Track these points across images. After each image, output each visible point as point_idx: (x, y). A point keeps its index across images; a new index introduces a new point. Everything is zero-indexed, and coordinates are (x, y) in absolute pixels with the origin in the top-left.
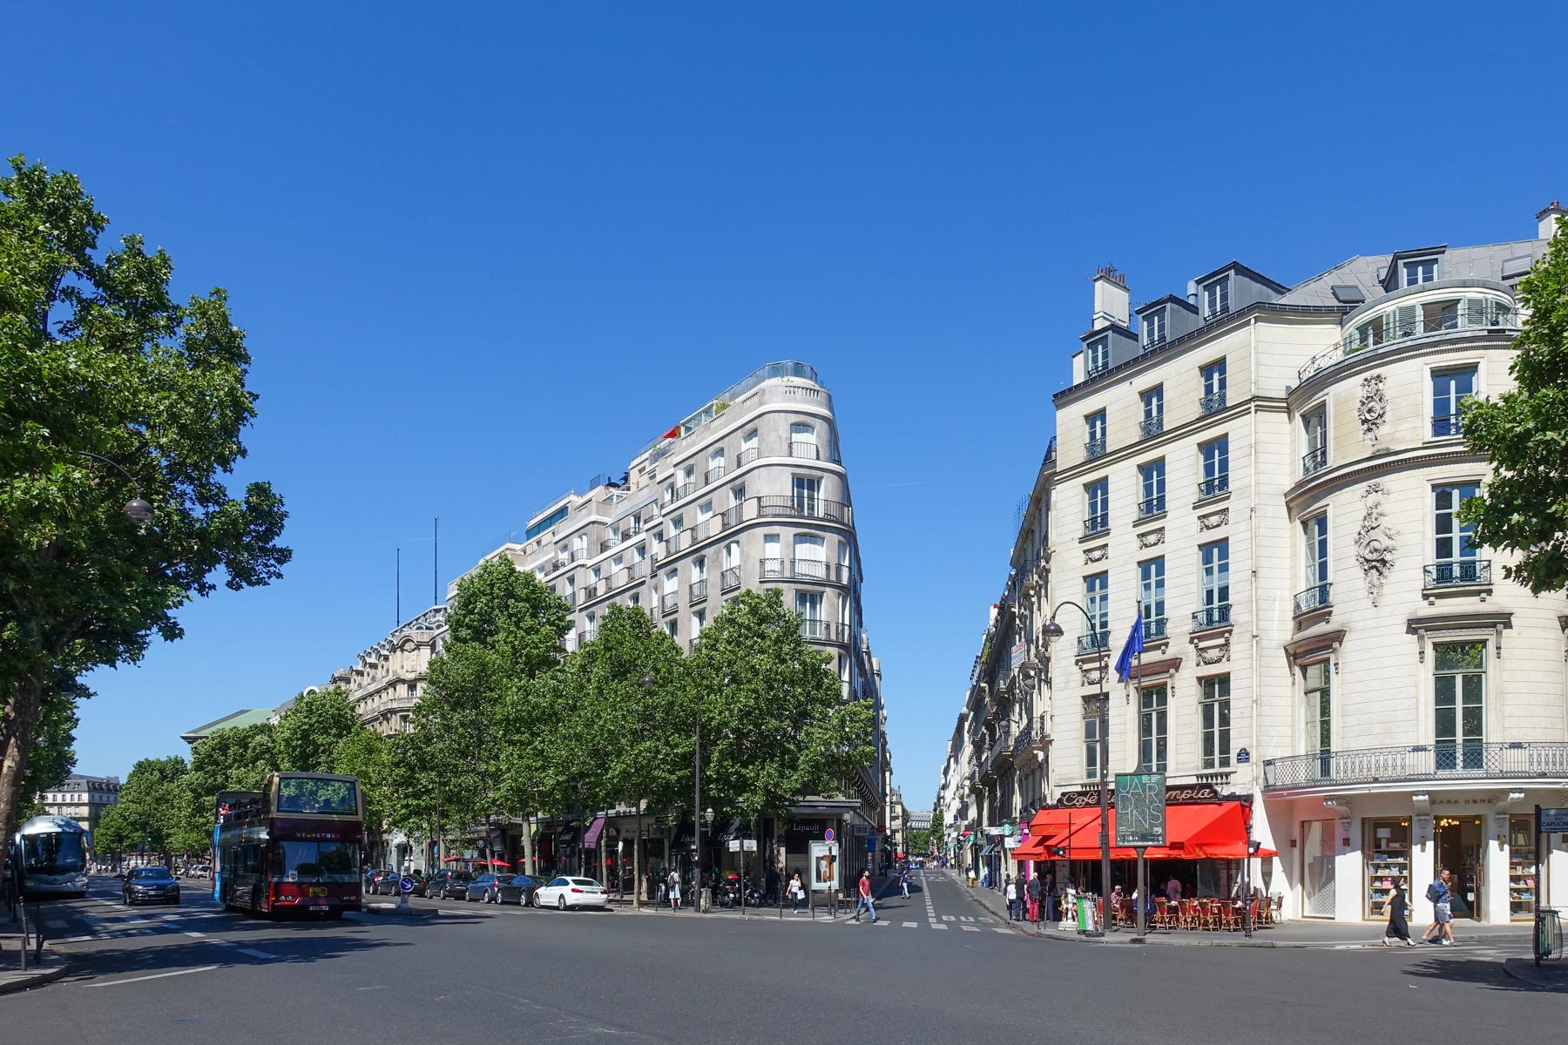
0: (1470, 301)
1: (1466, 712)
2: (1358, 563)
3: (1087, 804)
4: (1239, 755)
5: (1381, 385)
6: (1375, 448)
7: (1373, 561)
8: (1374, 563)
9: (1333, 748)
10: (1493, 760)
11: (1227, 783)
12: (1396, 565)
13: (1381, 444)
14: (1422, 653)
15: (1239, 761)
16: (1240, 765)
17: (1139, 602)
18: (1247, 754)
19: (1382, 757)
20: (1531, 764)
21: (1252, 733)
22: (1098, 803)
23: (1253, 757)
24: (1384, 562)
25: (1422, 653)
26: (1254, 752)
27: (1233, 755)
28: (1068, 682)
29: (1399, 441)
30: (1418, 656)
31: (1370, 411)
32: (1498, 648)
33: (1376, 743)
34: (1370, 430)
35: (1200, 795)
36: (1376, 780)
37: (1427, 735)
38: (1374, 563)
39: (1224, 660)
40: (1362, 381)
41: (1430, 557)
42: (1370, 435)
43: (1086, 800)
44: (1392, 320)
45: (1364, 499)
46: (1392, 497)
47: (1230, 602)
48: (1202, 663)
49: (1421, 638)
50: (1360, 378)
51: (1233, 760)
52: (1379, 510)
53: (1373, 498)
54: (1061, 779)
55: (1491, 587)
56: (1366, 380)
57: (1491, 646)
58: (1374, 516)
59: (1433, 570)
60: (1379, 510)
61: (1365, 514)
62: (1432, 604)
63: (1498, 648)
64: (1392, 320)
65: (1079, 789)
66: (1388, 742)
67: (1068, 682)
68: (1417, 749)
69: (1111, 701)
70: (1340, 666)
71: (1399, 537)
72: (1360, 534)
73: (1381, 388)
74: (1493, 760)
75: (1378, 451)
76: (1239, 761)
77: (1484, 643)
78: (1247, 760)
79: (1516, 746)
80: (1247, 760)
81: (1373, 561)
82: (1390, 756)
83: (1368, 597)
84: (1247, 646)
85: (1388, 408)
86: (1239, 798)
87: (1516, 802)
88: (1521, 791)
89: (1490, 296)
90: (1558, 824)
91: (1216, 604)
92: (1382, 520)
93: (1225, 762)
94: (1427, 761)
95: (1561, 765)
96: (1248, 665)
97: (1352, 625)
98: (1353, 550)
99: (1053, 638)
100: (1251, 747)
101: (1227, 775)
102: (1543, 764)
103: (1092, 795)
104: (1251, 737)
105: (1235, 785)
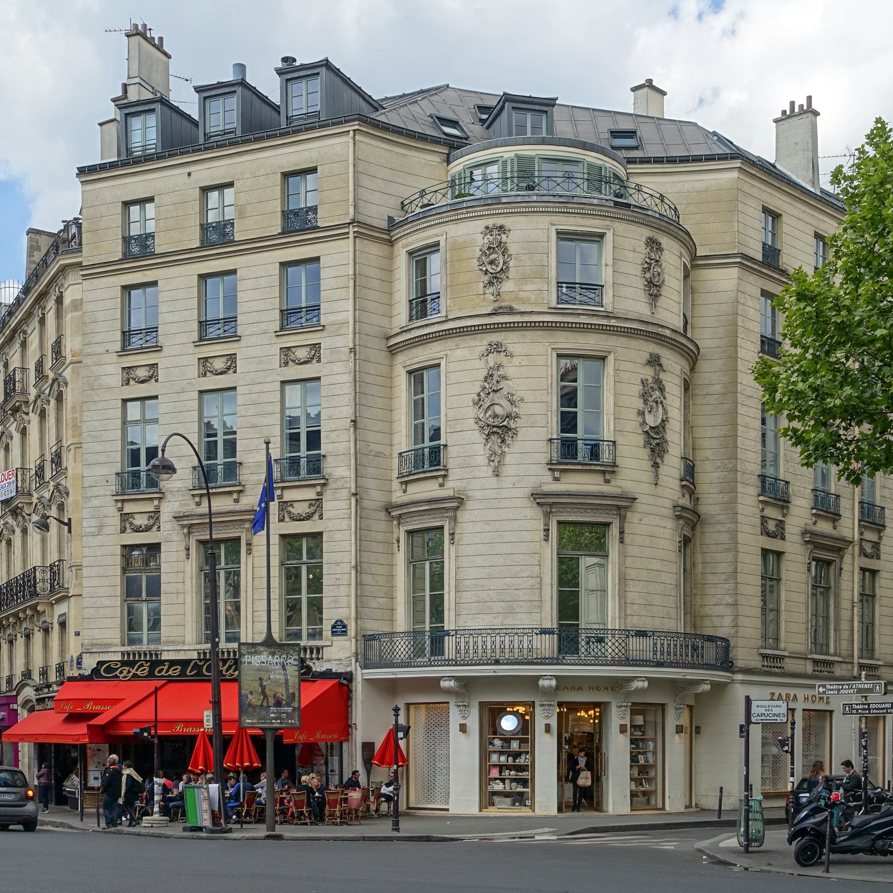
0: (590, 165)
1: (298, 591)
2: (476, 427)
3: (135, 675)
4: (334, 627)
5: (504, 237)
6: (496, 305)
7: (494, 427)
8: (495, 429)
9: (449, 624)
10: (617, 644)
11: (318, 659)
12: (519, 434)
13: (503, 301)
14: (547, 530)
15: (334, 633)
16: (335, 638)
17: (268, 443)
18: (344, 626)
19: (507, 637)
20: (655, 653)
21: (349, 603)
22: (151, 674)
23: (352, 631)
24: (507, 428)
25: (547, 530)
26: (353, 624)
27: (327, 626)
28: (101, 527)
29: (523, 301)
30: (542, 533)
31: (492, 262)
32: (622, 533)
33: (497, 622)
34: (491, 283)
35: (170, 673)
36: (497, 662)
37: (549, 617)
38: (495, 429)
39: (316, 517)
40: (482, 229)
41: (553, 427)
42: (491, 290)
43: (133, 671)
44: (509, 169)
45: (484, 359)
46: (516, 361)
47: (323, 451)
48: (287, 519)
49: (547, 515)
50: (480, 225)
51: (327, 633)
52: (501, 372)
53: (492, 359)
54: (93, 645)
55: (616, 469)
56: (487, 228)
57: (614, 531)
58: (495, 377)
59: (557, 444)
60: (501, 372)
61: (485, 373)
62: (556, 479)
63: (622, 533)
64: (509, 169)
65: (118, 657)
66: (509, 622)
67: (101, 527)
68: (543, 632)
69: (164, 556)
70: (456, 537)
71: (522, 405)
72: (479, 395)
73: (503, 240)
74: (620, 648)
75: (501, 308)
76: (334, 633)
77: (607, 525)
78: (344, 633)
79: (641, 634)
80: (344, 633)
81: (494, 427)
82: (526, 637)
83: (489, 465)
84: (344, 505)
85: (511, 264)
86: (338, 675)
87: (639, 691)
88: (451, 678)
89: (608, 165)
90: (768, 715)
91: (303, 452)
92: (503, 384)
93: (315, 634)
94: (547, 645)
95: (675, 655)
96: (345, 527)
97: (470, 493)
98: (471, 412)
99: (164, 476)
100: (349, 619)
101: (319, 649)
102: (659, 654)
103: (142, 665)
104: (349, 607)
105: (329, 661)
